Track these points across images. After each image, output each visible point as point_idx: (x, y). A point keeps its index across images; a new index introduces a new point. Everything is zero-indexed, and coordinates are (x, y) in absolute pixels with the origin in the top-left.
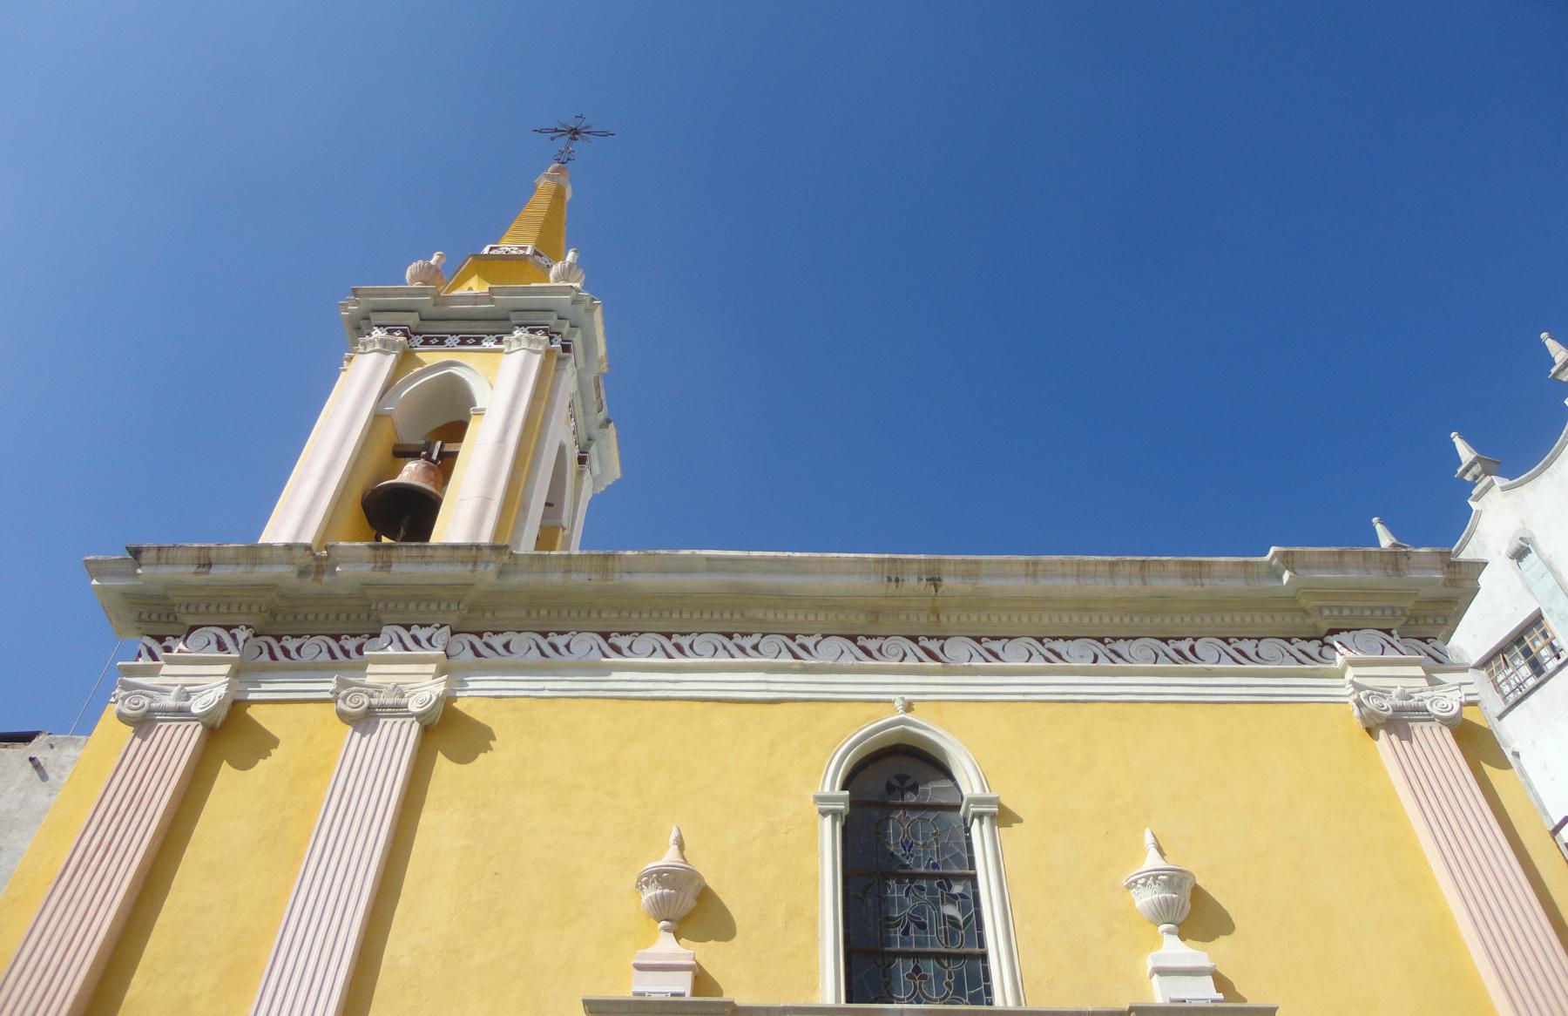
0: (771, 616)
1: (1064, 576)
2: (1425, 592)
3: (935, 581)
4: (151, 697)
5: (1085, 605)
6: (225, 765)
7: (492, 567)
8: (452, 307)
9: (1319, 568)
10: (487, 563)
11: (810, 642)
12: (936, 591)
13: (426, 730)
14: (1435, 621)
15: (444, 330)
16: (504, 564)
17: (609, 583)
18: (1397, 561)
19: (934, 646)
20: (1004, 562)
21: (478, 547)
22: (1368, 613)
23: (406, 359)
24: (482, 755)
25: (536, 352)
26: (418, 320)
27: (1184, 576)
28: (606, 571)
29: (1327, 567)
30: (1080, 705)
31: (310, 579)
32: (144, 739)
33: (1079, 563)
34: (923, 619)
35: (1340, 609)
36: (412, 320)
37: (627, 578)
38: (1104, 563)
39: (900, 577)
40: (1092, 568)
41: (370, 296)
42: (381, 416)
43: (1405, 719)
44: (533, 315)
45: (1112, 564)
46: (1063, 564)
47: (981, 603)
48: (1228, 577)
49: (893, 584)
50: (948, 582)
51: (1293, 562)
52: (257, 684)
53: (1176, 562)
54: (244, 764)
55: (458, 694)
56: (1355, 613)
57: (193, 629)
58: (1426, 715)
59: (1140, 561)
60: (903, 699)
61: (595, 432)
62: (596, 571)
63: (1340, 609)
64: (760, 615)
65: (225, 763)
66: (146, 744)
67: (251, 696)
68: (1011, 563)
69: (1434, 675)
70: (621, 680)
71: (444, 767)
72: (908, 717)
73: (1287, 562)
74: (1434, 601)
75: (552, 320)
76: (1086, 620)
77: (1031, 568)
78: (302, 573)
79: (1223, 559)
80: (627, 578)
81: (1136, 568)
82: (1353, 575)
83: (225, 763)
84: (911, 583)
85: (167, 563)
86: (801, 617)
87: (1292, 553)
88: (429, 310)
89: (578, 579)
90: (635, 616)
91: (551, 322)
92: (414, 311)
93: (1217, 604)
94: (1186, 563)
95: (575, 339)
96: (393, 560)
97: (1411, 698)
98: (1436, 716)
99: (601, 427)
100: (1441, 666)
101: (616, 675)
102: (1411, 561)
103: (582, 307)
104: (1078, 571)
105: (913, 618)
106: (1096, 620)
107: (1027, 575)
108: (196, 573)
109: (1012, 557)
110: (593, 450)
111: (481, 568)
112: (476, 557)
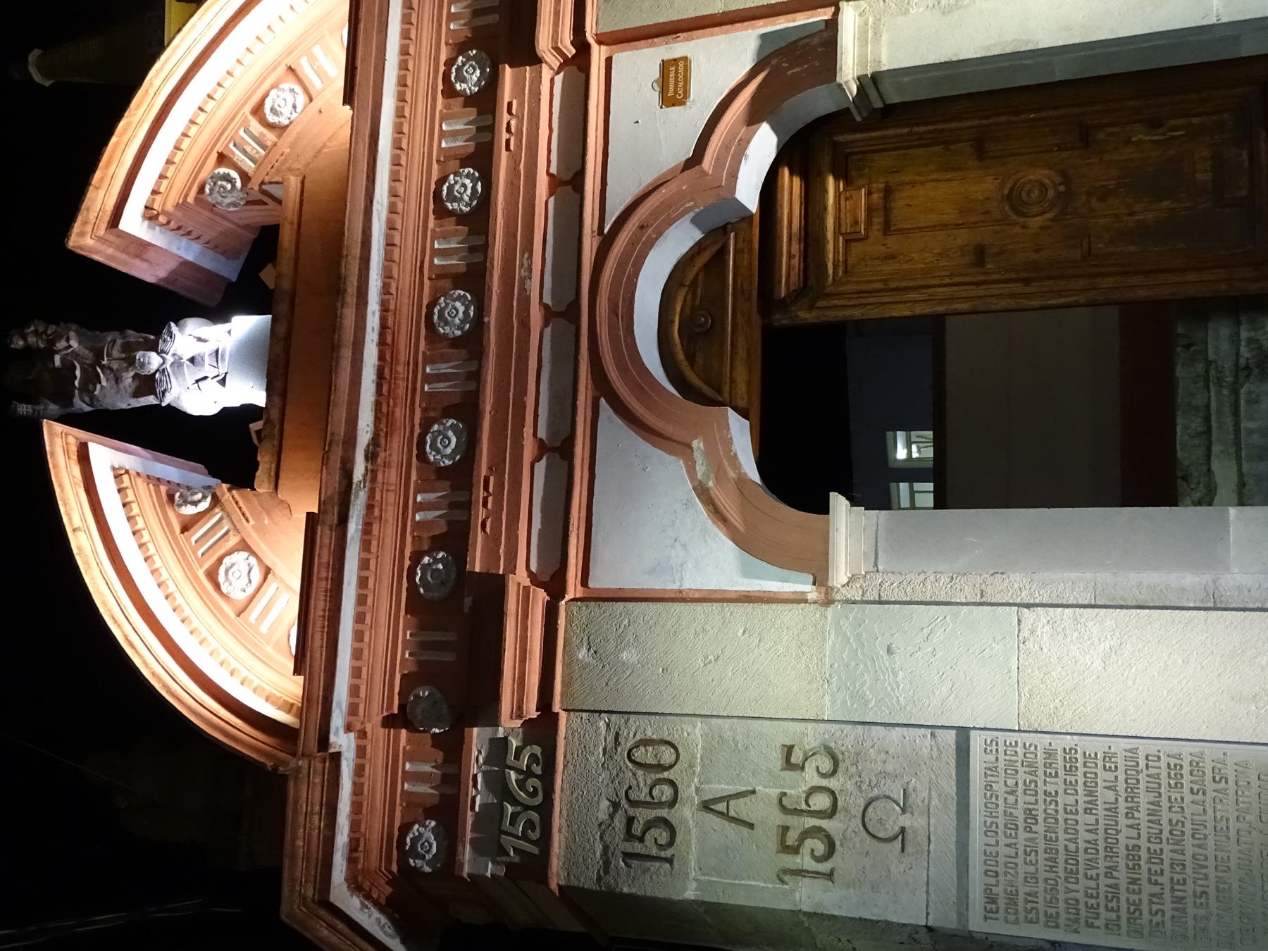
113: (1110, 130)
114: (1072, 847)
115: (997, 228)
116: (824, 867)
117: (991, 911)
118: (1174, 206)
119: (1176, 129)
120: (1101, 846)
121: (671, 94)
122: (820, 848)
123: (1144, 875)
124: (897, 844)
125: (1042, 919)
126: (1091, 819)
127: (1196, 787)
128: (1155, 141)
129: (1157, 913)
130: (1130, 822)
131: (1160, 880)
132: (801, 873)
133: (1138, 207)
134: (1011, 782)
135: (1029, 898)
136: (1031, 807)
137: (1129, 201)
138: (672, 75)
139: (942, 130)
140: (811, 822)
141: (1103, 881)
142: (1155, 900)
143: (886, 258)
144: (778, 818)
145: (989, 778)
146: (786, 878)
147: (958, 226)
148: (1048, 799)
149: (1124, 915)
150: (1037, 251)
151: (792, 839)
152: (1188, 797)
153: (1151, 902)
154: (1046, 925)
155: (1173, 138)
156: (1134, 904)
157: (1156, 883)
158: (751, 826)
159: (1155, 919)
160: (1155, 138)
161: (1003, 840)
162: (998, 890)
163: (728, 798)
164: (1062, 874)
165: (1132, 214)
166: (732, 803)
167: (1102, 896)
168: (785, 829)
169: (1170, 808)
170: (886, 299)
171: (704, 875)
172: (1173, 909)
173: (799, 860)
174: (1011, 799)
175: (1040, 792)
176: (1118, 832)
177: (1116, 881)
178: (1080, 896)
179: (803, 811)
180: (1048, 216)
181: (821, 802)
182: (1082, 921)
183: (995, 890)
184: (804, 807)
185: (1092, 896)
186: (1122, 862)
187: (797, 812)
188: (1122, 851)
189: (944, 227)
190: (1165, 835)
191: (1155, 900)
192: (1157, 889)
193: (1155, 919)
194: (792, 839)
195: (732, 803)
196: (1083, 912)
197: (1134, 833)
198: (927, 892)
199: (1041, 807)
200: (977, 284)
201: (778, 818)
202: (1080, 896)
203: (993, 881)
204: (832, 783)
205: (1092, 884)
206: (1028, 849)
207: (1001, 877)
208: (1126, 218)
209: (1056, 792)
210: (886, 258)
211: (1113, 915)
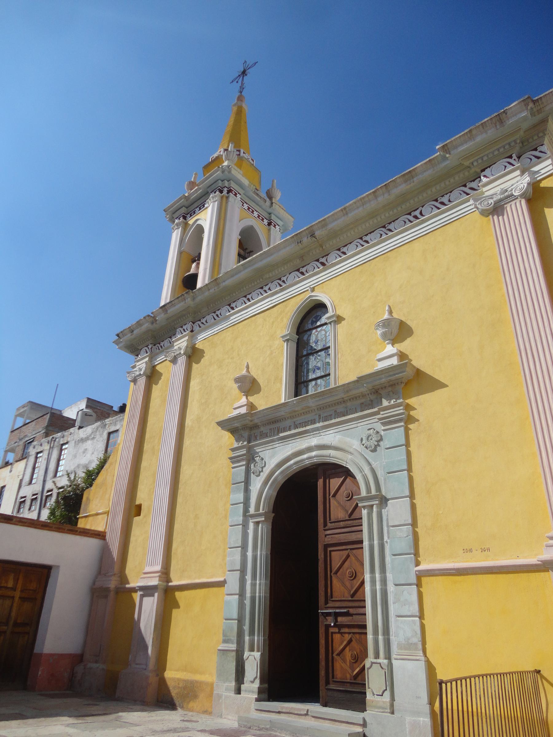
0: (271, 275)
1: (358, 208)
2: (525, 126)
3: (313, 235)
4: (134, 373)
5: (372, 215)
6: (154, 385)
7: (189, 299)
8: (191, 198)
9: (462, 144)
10: (187, 298)
11: (284, 279)
12: (316, 239)
13: (530, 201)
14: (538, 136)
15: (193, 208)
16: (193, 296)
17: (220, 288)
18: (500, 119)
19: (323, 260)
20: (333, 215)
21: (207, 285)
22: (496, 153)
23: (186, 226)
24: (202, 359)
25: (215, 201)
26: (186, 209)
27: (406, 181)
28: (218, 284)
29: (466, 142)
30: (371, 261)
31: (154, 324)
32: (503, 215)
33: (361, 199)
34: (318, 251)
35: (482, 158)
36: (183, 210)
37: (224, 284)
38: (370, 194)
39: (301, 240)
40: (367, 199)
41: (169, 209)
42: (182, 252)
43: (502, 205)
44: (213, 186)
45: (374, 192)
46: (355, 203)
47: (334, 234)
48: (425, 171)
49: (299, 244)
50: (317, 233)
51: (448, 149)
52: (156, 359)
53: (399, 177)
54: (198, 362)
55: (196, 342)
56: (490, 157)
57: (141, 349)
58: (514, 197)
59: (384, 185)
60: (310, 288)
61: (270, 210)
62: (216, 286)
63: (482, 158)
64: (268, 276)
65: (154, 385)
66: (505, 217)
67: (156, 363)
68: (336, 213)
69: (532, 169)
70: (234, 318)
71: (195, 366)
72: (313, 294)
73: (446, 150)
74: (535, 126)
75: (220, 184)
76: (375, 221)
77: (344, 212)
78: (152, 323)
79: (419, 164)
80: (224, 284)
81: (384, 189)
82: (479, 139)
83: (154, 385)
84: (305, 240)
85: (126, 335)
86: (280, 270)
87: (446, 145)
88: (187, 204)
89: (212, 291)
90: (234, 294)
91: (220, 185)
92: (182, 207)
93: (426, 186)
94: (404, 175)
95: (232, 185)
96: (167, 309)
97: (507, 191)
98: (518, 196)
99: (270, 207)
100: (540, 160)
101: (232, 318)
102: (507, 115)
103: (226, 172)
104: (362, 203)
105: (314, 253)
106: (379, 219)
107: (344, 215)
108: (131, 335)
109: (336, 211)
110: (273, 217)
111: (186, 301)
112: (184, 298)
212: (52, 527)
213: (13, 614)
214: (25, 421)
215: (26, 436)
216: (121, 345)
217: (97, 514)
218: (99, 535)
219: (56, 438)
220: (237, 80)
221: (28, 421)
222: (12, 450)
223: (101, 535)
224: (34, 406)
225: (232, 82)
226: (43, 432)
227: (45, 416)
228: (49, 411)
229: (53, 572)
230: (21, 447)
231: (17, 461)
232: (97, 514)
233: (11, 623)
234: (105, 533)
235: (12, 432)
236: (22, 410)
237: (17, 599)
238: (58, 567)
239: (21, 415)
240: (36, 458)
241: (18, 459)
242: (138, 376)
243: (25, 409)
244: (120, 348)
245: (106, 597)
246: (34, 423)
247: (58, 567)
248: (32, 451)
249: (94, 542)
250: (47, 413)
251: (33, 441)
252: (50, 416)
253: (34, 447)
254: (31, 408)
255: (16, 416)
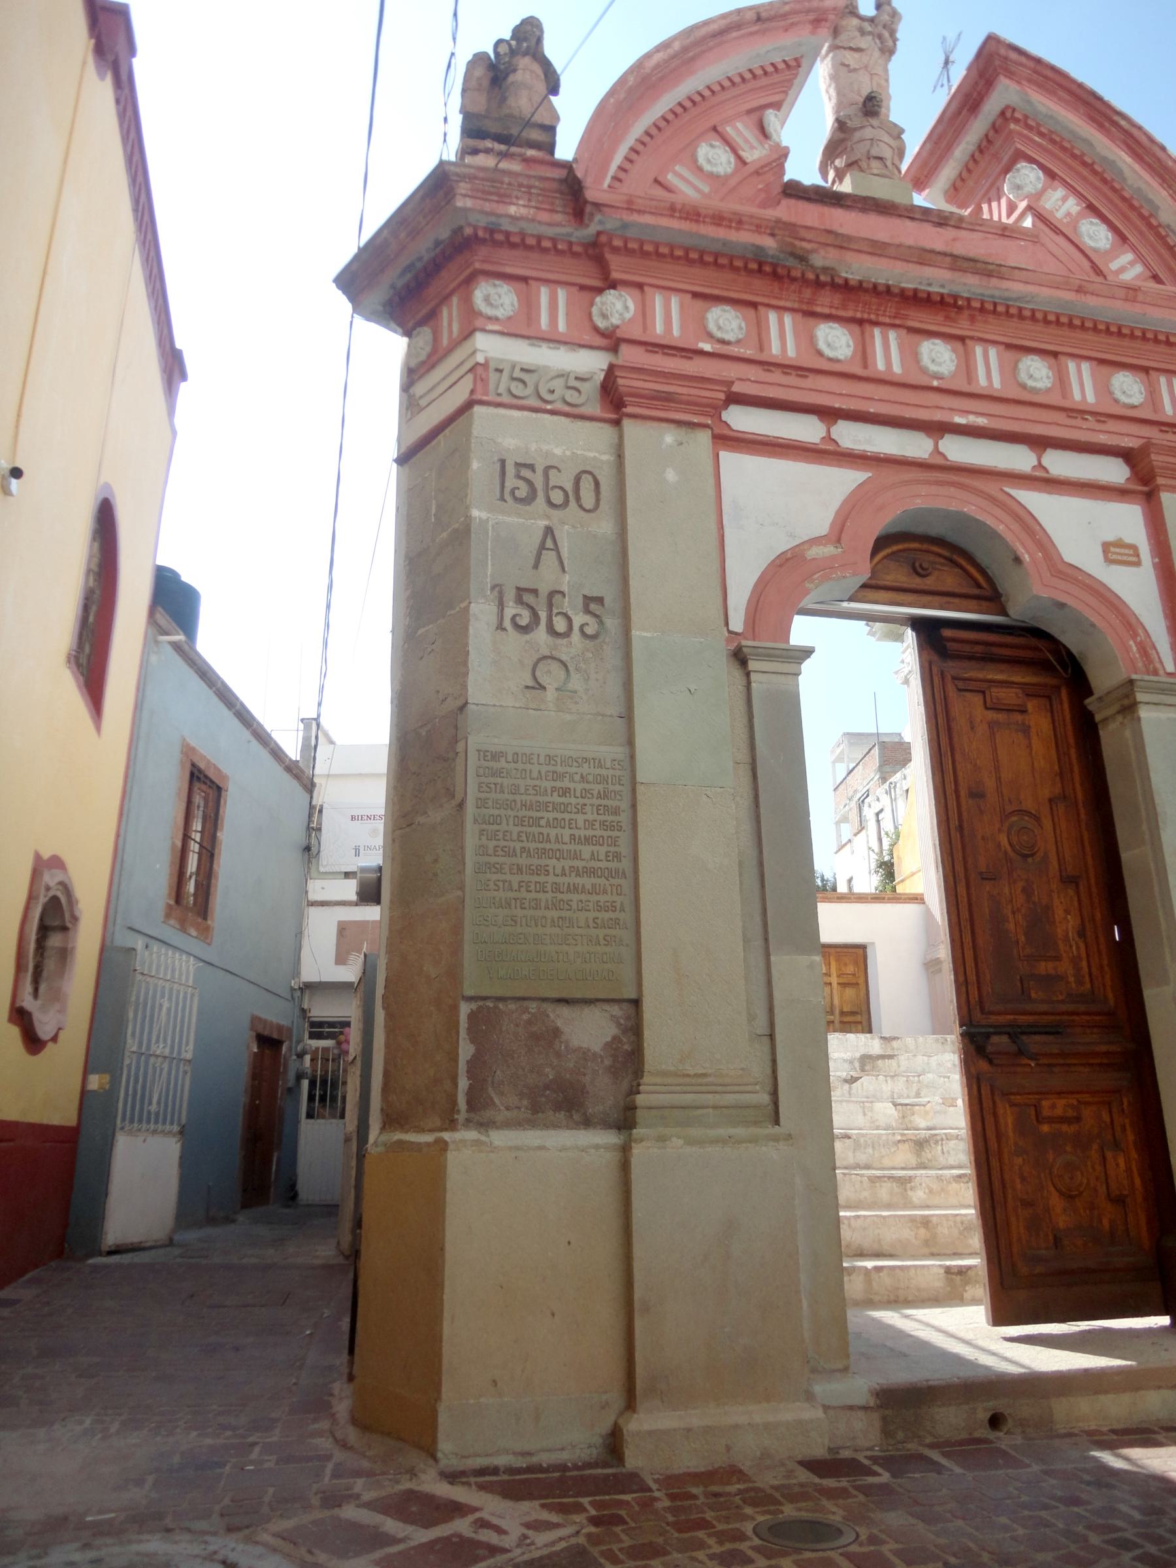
113: (1076, 899)
114: (543, 822)
115: (998, 809)
116: (507, 623)
117: (485, 756)
118: (1021, 944)
119: (1078, 948)
120: (548, 846)
121: (1112, 549)
122: (524, 621)
123: (526, 878)
124: (531, 683)
125: (483, 795)
126: (566, 839)
127: (599, 921)
128: (1068, 933)
129: (496, 885)
130: (567, 868)
131: (523, 889)
132: (501, 605)
133: (1020, 917)
134: (590, 778)
135: (498, 786)
136: (572, 792)
137: (1023, 911)
138: (1127, 551)
139: (1072, 771)
140: (543, 615)
141: (518, 845)
142: (507, 884)
143: (971, 722)
144: (544, 590)
145: (592, 761)
146: (496, 593)
147: (999, 779)
148: (579, 807)
149: (493, 859)
150: (983, 838)
151: (528, 598)
152: (591, 915)
153: (504, 881)
154: (478, 799)
155: (1071, 946)
156: (501, 869)
157: (520, 887)
158: (536, 566)
159: (491, 883)
160: (1070, 934)
161: (544, 769)
162: (502, 763)
163: (557, 549)
164: (520, 814)
165: (1013, 913)
166: (554, 553)
167: (505, 843)
168: (535, 592)
169: (581, 901)
170: (940, 720)
171: (493, 526)
172: (501, 899)
173: (511, 604)
174: (577, 778)
175: (586, 801)
176: (558, 859)
177: (519, 854)
178: (504, 827)
179: (551, 611)
180: (1009, 849)
181: (560, 625)
182: (484, 826)
183: (503, 760)
184: (555, 611)
185: (504, 835)
186: (536, 861)
187: (550, 606)
188: (543, 862)
189: (997, 769)
190: (560, 896)
191: (507, 884)
192: (515, 886)
193: (491, 883)
194: (528, 598)
195: (554, 553)
196: (492, 827)
197: (559, 871)
198: (494, 705)
199: (573, 801)
200: (957, 791)
201: (544, 590)
202: (504, 827)
203: (510, 758)
204: (576, 635)
205: (515, 836)
206: (538, 789)
207: (513, 765)
208: (1010, 907)
209: (585, 813)
210: (971, 722)
211: (491, 851)
212: (850, 898)
213: (836, 1002)
214: (848, 767)
215: (855, 791)
216: (877, 636)
217: (913, 874)
218: (917, 899)
219: (896, 783)
220: (940, 84)
221: (852, 766)
222: (845, 819)
223: (917, 899)
224: (854, 738)
225: (935, 88)
226: (877, 777)
227: (872, 751)
228: (874, 740)
229: (869, 950)
230: (855, 811)
231: (855, 835)
232: (913, 874)
233: (837, 1012)
234: (923, 895)
235: (835, 789)
236: (838, 751)
237: (835, 985)
238: (873, 944)
239: (839, 759)
240: (878, 821)
241: (856, 831)
242: (908, 674)
243: (841, 747)
244: (878, 640)
245: (940, 971)
246: (860, 767)
247: (873, 944)
248: (869, 813)
249: (911, 909)
250: (874, 746)
251: (868, 795)
252: (879, 749)
253: (870, 806)
254: (851, 744)
255: (834, 762)
